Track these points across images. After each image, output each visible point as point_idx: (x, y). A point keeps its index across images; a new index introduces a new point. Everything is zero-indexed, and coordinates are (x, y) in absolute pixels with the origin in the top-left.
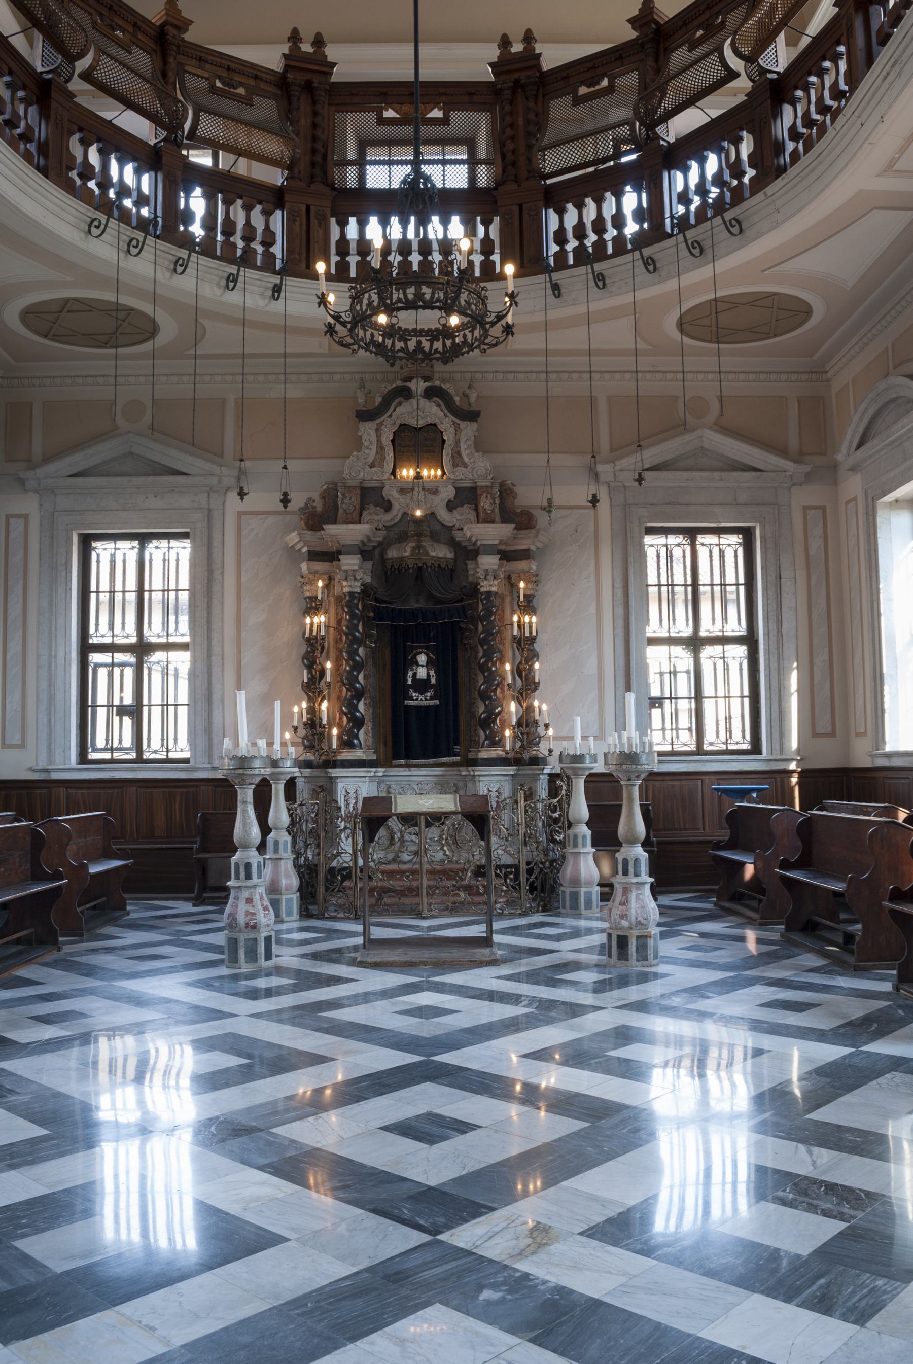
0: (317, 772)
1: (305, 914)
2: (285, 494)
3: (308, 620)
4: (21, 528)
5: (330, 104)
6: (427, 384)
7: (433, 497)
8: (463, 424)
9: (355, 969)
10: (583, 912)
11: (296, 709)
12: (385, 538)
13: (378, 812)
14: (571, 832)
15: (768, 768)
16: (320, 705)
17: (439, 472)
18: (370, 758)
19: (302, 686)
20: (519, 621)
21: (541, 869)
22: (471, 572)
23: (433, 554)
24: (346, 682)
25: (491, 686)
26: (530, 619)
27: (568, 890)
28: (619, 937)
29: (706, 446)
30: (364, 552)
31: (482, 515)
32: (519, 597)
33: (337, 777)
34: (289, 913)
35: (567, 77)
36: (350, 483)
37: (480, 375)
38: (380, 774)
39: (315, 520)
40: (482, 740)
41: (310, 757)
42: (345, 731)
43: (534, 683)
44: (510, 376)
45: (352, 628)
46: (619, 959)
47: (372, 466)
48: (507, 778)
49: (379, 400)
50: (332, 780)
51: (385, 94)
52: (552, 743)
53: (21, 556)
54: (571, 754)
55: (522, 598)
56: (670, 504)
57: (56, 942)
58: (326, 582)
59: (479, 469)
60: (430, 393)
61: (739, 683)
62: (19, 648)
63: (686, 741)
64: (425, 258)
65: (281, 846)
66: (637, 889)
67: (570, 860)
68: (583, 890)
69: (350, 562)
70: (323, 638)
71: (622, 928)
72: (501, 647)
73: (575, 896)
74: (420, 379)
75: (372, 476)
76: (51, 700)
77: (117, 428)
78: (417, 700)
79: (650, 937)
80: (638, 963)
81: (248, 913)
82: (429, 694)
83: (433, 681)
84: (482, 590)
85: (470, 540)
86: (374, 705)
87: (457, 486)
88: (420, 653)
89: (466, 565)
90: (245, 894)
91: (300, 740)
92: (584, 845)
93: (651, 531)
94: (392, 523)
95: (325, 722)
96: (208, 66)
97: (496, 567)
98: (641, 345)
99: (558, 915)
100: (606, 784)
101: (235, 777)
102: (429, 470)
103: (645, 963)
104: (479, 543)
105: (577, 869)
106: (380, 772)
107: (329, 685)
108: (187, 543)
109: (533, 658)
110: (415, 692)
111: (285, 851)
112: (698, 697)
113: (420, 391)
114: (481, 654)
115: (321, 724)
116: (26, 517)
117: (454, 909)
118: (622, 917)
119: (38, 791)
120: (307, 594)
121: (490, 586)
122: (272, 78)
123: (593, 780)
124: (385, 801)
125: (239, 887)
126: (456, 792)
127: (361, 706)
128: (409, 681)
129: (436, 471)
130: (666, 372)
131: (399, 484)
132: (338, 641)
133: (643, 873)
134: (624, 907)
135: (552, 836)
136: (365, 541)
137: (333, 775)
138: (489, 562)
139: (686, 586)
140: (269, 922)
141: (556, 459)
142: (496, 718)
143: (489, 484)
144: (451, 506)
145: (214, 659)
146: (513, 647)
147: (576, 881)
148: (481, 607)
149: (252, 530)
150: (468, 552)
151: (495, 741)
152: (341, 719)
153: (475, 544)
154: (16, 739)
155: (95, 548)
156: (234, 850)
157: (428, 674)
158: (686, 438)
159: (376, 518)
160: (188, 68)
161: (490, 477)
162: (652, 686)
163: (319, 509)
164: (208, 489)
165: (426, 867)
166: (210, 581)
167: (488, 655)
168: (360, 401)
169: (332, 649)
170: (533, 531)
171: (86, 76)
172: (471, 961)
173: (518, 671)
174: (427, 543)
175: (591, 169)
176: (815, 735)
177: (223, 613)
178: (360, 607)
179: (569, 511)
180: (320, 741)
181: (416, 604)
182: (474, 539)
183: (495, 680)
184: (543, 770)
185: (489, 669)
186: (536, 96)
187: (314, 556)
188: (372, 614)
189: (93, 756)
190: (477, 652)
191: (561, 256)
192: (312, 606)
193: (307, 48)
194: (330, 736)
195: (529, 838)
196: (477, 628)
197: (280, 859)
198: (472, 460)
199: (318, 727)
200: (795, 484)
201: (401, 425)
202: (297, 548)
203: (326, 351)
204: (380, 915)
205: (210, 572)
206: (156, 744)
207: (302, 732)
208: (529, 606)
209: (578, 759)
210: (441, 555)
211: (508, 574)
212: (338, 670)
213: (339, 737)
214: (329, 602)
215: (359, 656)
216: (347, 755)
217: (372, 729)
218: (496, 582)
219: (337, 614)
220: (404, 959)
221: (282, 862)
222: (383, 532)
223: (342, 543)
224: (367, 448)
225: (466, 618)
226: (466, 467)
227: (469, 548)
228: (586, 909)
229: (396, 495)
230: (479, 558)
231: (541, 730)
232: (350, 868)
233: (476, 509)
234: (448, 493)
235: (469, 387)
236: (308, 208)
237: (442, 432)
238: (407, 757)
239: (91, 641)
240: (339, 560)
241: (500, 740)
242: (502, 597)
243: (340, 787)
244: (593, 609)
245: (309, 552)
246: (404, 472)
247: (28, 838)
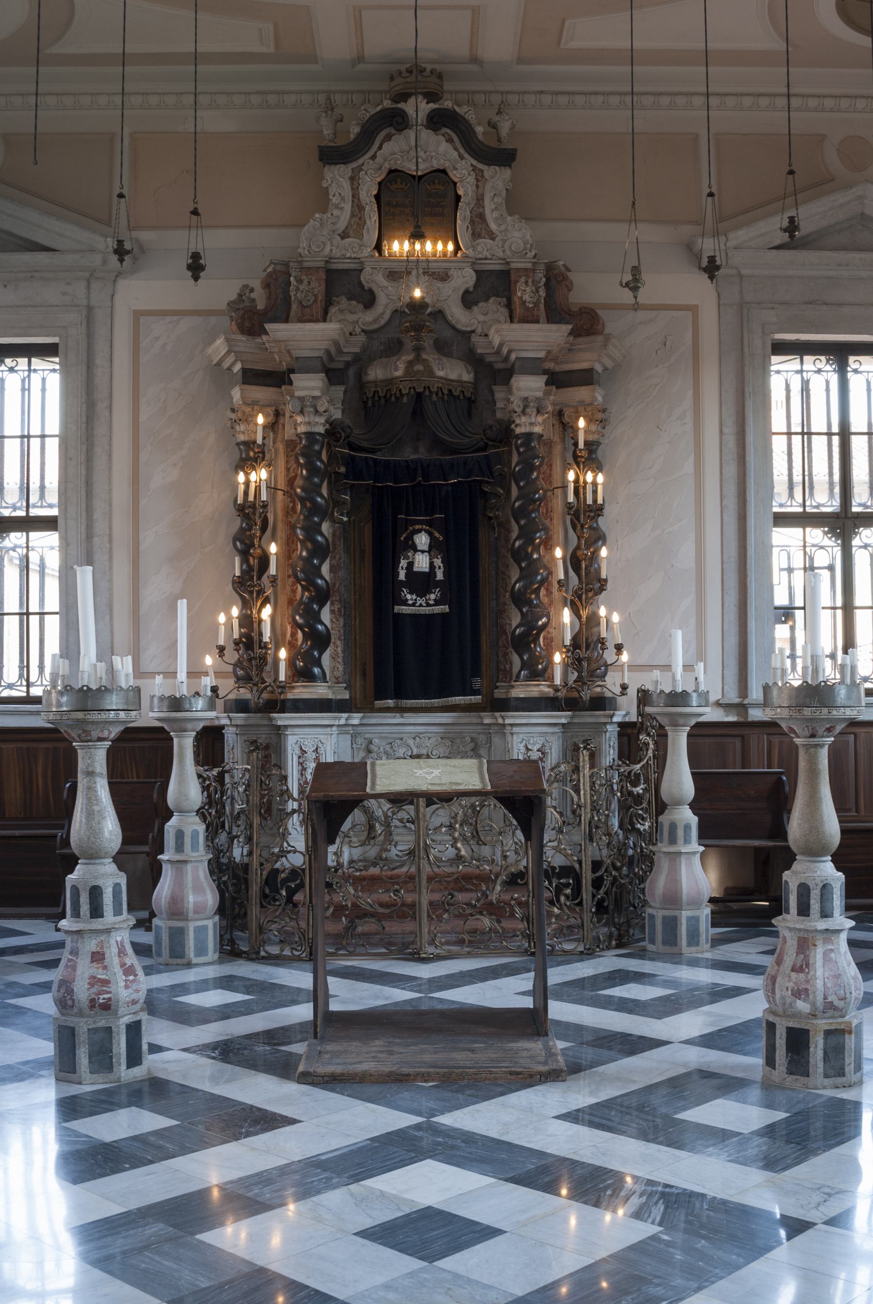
0: (255, 718)
1: (230, 950)
2: (196, 256)
3: (241, 478)
6: (432, 106)
7: (440, 285)
8: (489, 171)
9: (292, 1088)
10: (688, 951)
11: (222, 618)
12: (364, 349)
13: (339, 791)
14: (664, 819)
16: (259, 611)
17: (451, 247)
18: (339, 697)
19: (234, 582)
20: (576, 481)
21: (615, 878)
22: (500, 405)
23: (441, 373)
24: (301, 575)
25: (532, 583)
26: (595, 477)
27: (659, 914)
28: (790, 1031)
30: (333, 375)
31: (518, 311)
32: (576, 444)
33: (286, 727)
34: (201, 951)
37: (516, 97)
38: (355, 722)
39: (250, 320)
40: (516, 670)
41: (245, 694)
42: (299, 653)
43: (600, 580)
44: (563, 100)
45: (312, 490)
46: (790, 1072)
47: (344, 235)
48: (556, 729)
49: (355, 130)
50: (279, 732)
52: (626, 674)
54: (667, 691)
55: (581, 445)
56: (811, 303)
58: (271, 419)
59: (513, 240)
60: (440, 120)
65: (188, 840)
66: (826, 941)
67: (663, 866)
68: (685, 914)
69: (309, 384)
70: (265, 506)
71: (797, 1015)
72: (547, 522)
73: (671, 924)
74: (420, 98)
75: (344, 252)
78: (413, 605)
79: (850, 1032)
80: (826, 1081)
81: (94, 981)
82: (433, 596)
83: (440, 576)
84: (518, 431)
85: (498, 352)
86: (344, 612)
87: (478, 268)
88: (419, 531)
89: (492, 393)
90: (91, 945)
91: (230, 669)
92: (687, 841)
93: (781, 348)
94: (376, 326)
95: (266, 638)
97: (540, 394)
99: (642, 954)
100: (707, 740)
101: (70, 726)
102: (435, 244)
103: (840, 1080)
104: (513, 356)
105: (674, 880)
106: (356, 719)
107: (274, 580)
108: (54, 363)
109: (596, 541)
110: (411, 593)
111: (195, 847)
113: (422, 116)
114: (515, 534)
115: (261, 641)
117: (474, 943)
118: (798, 993)
120: (242, 438)
121: (531, 424)
123: (701, 732)
124: (356, 772)
125: (78, 932)
126: (475, 752)
127: (326, 615)
128: (402, 576)
129: (445, 245)
130: (808, 96)
131: (387, 265)
132: (289, 511)
134: (802, 976)
135: (632, 824)
136: (333, 351)
137: (280, 723)
138: (529, 385)
139: (829, 434)
140: (135, 996)
142: (538, 635)
143: (530, 266)
144: (468, 300)
145: (96, 540)
146: (564, 523)
147: (673, 900)
148: (515, 458)
149: (157, 339)
150: (496, 372)
151: (537, 671)
152: (293, 635)
153: (506, 359)
157: (432, 565)
158: (840, 198)
159: (352, 317)
161: (530, 255)
162: (777, 590)
163: (261, 305)
164: (87, 274)
165: (427, 869)
167: (527, 535)
168: (325, 132)
169: (280, 525)
170: (600, 338)
172: (511, 1073)
173: (574, 561)
174: (430, 356)
177: (110, 468)
178: (324, 456)
179: (653, 314)
180: (261, 668)
182: (505, 350)
183: (537, 573)
184: (612, 716)
185: (528, 557)
187: (253, 377)
188: (343, 470)
190: (509, 531)
192: (249, 456)
194: (276, 661)
195: (597, 827)
196: (508, 492)
197: (186, 862)
198: (503, 227)
199: (256, 646)
201: (391, 171)
202: (226, 365)
203: (272, 50)
204: (351, 954)
207: (232, 656)
208: (590, 457)
209: (678, 698)
210: (453, 376)
211: (558, 408)
212: (289, 557)
213: (291, 662)
214: (276, 451)
215: (322, 535)
216: (302, 691)
217: (344, 651)
218: (540, 419)
219: (288, 469)
220: (386, 1069)
221: (189, 867)
222: (363, 338)
223: (296, 353)
224: (337, 206)
225: (493, 477)
226: (493, 239)
227: (498, 366)
228: (689, 945)
229: (384, 282)
230: (513, 380)
231: (609, 656)
233: (509, 305)
234: (465, 279)
235: (499, 113)
237: (455, 184)
238: (398, 696)
240: (291, 383)
241: (545, 669)
242: (549, 444)
243: (292, 742)
244: (689, 467)
245: (244, 371)
246: (396, 246)
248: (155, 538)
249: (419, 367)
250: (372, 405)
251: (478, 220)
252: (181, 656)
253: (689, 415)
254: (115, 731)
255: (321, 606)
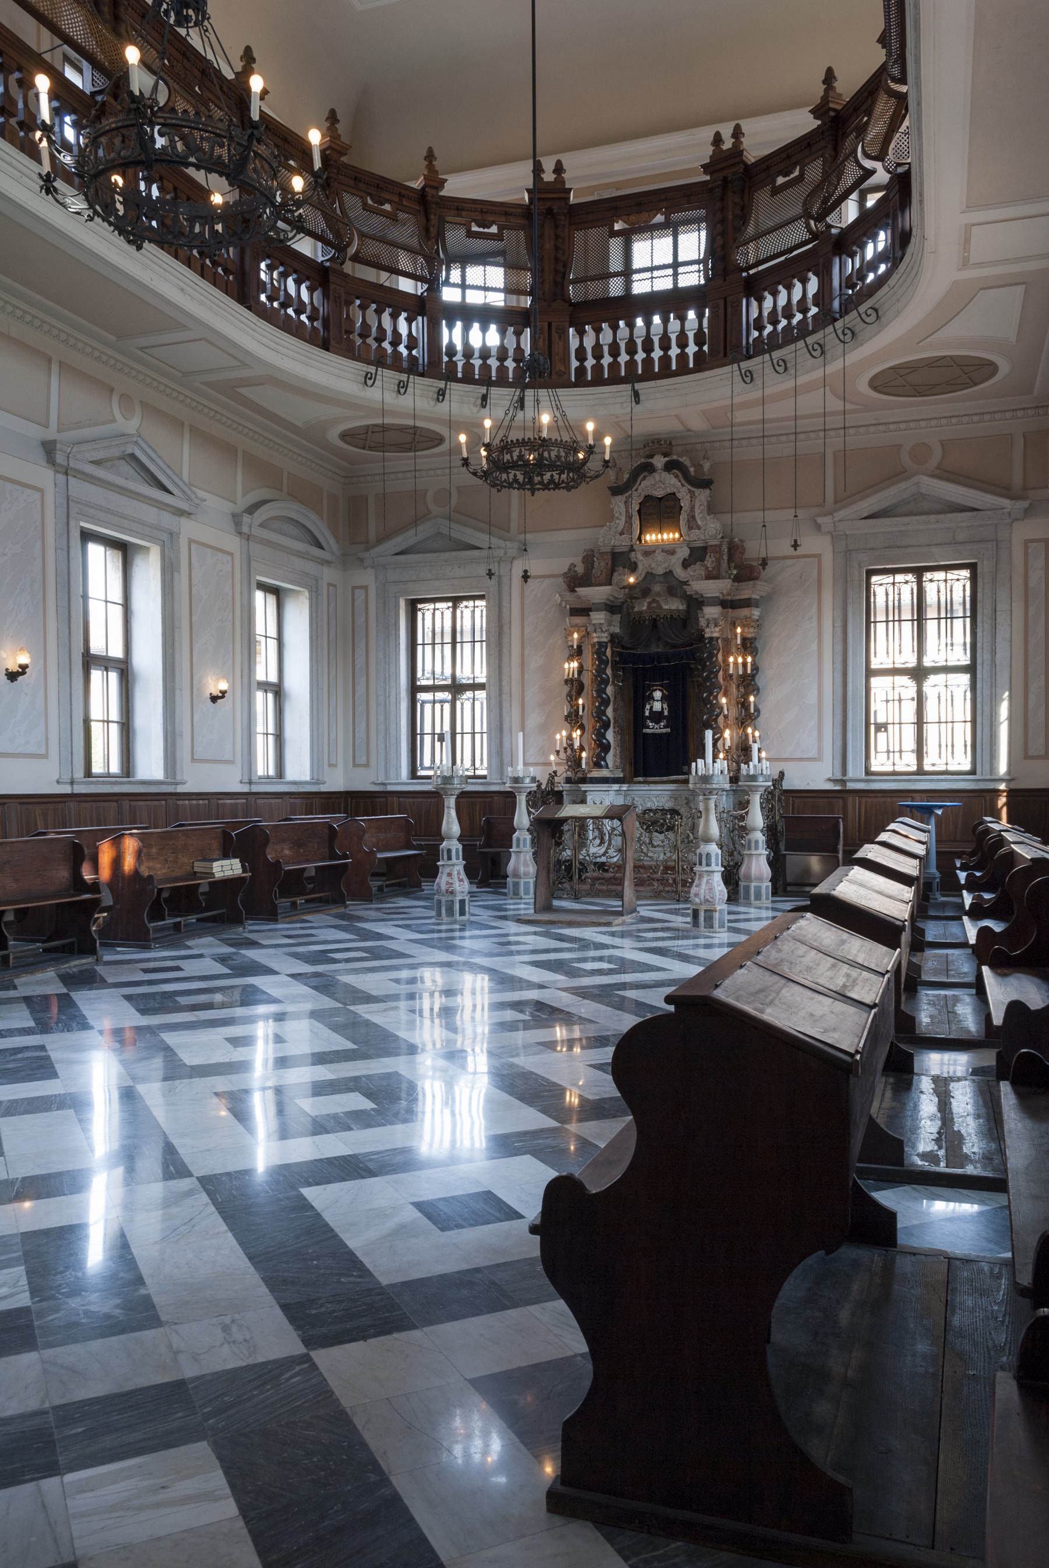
2: (526, 571)
4: (363, 597)
5: (570, 224)
6: (667, 459)
8: (697, 491)
15: (977, 787)
17: (677, 535)
23: (667, 607)
29: (923, 491)
30: (611, 608)
35: (768, 168)
36: (603, 550)
39: (574, 581)
47: (621, 534)
49: (626, 476)
51: (615, 208)
53: (363, 619)
57: (344, 903)
59: (710, 529)
60: (669, 467)
61: (962, 710)
62: (364, 690)
63: (908, 763)
64: (502, 365)
65: (521, 842)
68: (753, 885)
69: (598, 617)
71: (696, 904)
75: (622, 542)
76: (387, 729)
77: (430, 512)
81: (447, 883)
83: (666, 713)
86: (620, 732)
90: (447, 870)
96: (464, 213)
98: (848, 406)
105: (749, 868)
106: (625, 787)
108: (481, 603)
112: (920, 723)
116: (366, 588)
119: (378, 800)
122: (520, 211)
128: (647, 713)
133: (713, 864)
138: (711, 612)
141: (770, 515)
144: (686, 564)
150: (696, 603)
154: (363, 760)
155: (420, 610)
156: (443, 840)
158: (903, 485)
160: (449, 219)
166: (500, 635)
171: (356, 259)
175: (783, 258)
176: (1027, 757)
179: (795, 561)
181: (656, 649)
185: (710, 702)
186: (743, 191)
187: (575, 612)
189: (421, 773)
191: (581, 371)
193: (549, 176)
200: (1016, 520)
205: (501, 627)
206: (468, 764)
210: (674, 607)
218: (717, 629)
221: (522, 855)
228: (756, 899)
232: (571, 861)
234: (684, 553)
236: (550, 325)
238: (645, 775)
239: (418, 683)
244: (814, 647)
245: (571, 609)
246: (648, 537)
247: (326, 831)
248: (532, 694)
249: (655, 605)
250: (635, 626)
251: (692, 518)
252: (537, 754)
253: (815, 617)
254: (457, 792)
255: (606, 730)
